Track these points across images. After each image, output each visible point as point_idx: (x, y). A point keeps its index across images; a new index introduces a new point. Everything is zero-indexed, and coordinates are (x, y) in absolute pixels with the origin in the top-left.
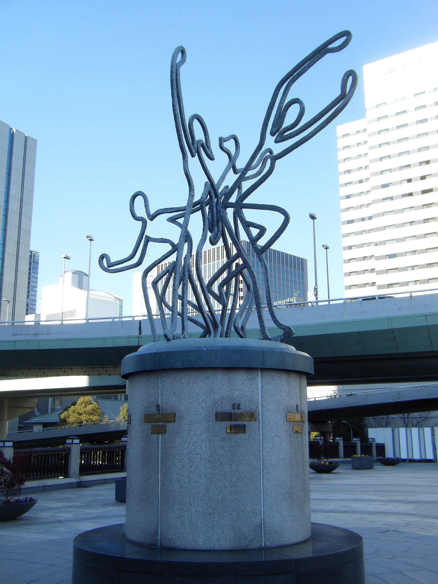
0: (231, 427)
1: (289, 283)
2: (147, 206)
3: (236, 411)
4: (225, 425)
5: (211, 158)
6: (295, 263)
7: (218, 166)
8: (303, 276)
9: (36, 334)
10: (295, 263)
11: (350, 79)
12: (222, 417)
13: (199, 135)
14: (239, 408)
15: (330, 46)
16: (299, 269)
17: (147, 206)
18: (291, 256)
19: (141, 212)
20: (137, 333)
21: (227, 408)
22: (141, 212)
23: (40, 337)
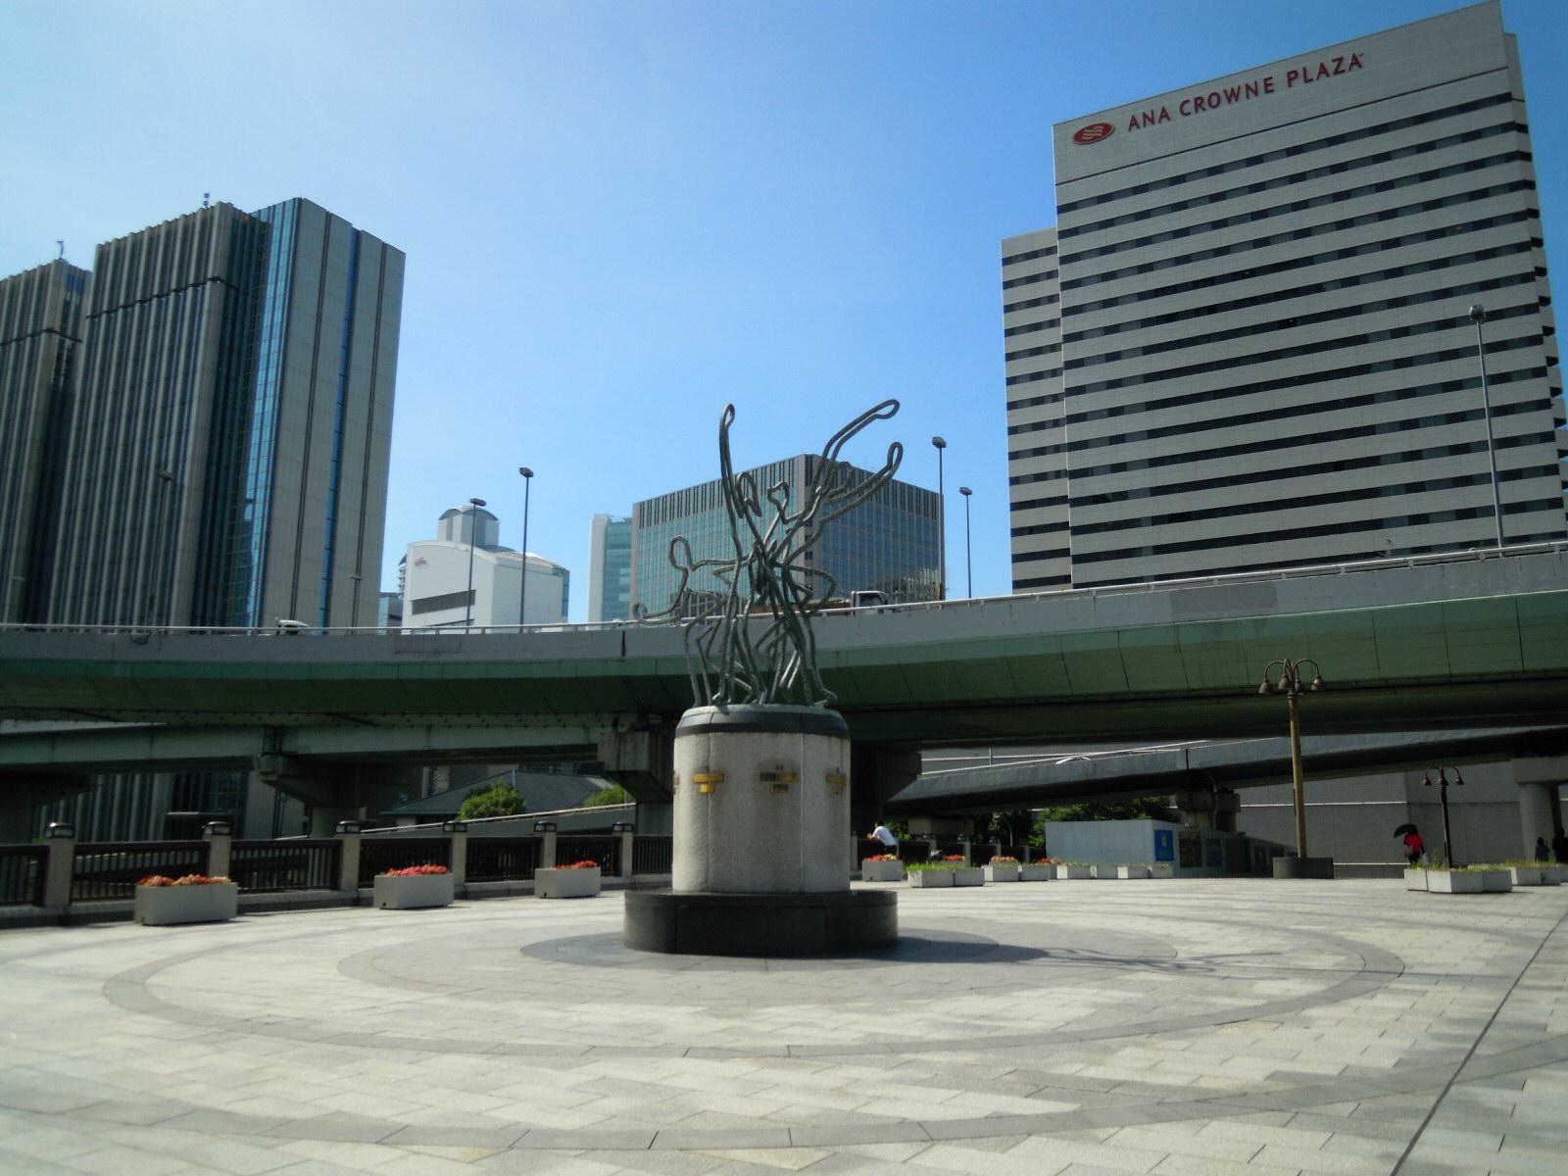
0: (775, 786)
1: (891, 568)
2: (688, 553)
3: (779, 772)
4: (768, 784)
5: (758, 513)
6: (918, 502)
7: (769, 526)
8: (935, 529)
9: (438, 652)
10: (918, 502)
11: (896, 450)
12: (767, 777)
13: (748, 496)
14: (782, 768)
15: (879, 412)
16: (926, 515)
17: (688, 553)
18: (911, 487)
19: (682, 561)
20: (617, 653)
21: (771, 770)
22: (682, 561)
23: (443, 658)
